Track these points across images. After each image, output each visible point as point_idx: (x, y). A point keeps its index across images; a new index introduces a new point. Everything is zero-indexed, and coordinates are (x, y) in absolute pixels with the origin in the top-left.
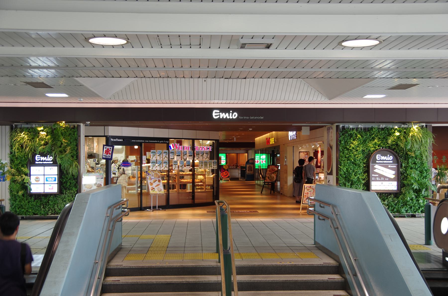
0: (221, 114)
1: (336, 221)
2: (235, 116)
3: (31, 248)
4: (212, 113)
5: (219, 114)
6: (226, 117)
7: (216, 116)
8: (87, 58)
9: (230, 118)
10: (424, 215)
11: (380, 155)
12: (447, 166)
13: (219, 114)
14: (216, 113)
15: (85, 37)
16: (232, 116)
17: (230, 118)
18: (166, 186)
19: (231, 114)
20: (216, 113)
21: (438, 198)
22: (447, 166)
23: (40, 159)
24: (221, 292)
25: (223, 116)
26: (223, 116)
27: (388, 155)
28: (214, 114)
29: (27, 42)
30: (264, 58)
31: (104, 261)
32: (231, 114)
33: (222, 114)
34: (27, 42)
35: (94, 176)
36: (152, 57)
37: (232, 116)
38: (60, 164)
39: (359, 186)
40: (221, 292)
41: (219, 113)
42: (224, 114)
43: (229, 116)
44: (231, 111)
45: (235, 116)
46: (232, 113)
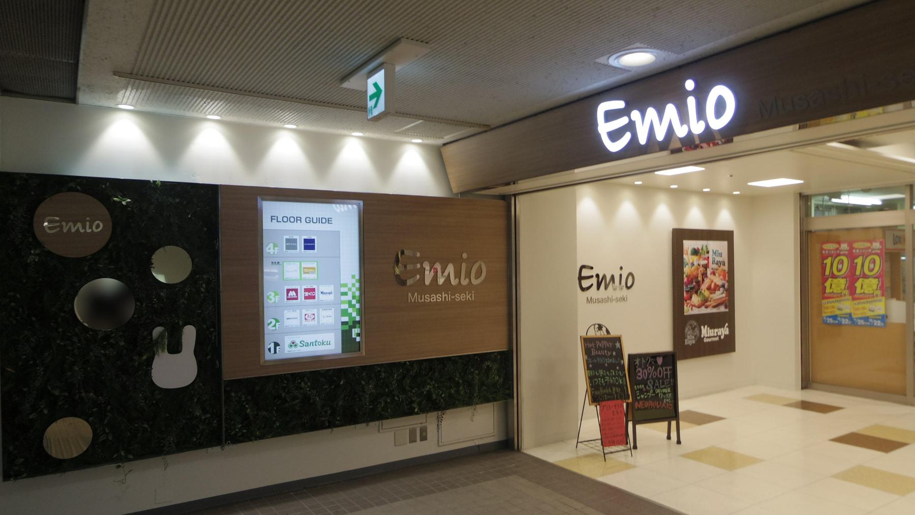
0: (635, 115)
3: (850, 196)
5: (624, 121)
6: (670, 131)
9: (690, 132)
10: (669, 391)
11: (620, 104)
12: (268, 294)
14: (611, 116)
17: (690, 132)
18: (901, 291)
20: (611, 116)
22: (268, 294)
23: (627, 137)
24: (269, 208)
27: (690, 85)
32: (691, 101)
36: (516, 374)
37: (701, 114)
38: (397, 265)
39: (14, 233)
40: (269, 208)
44: (690, 85)
46: (701, 94)
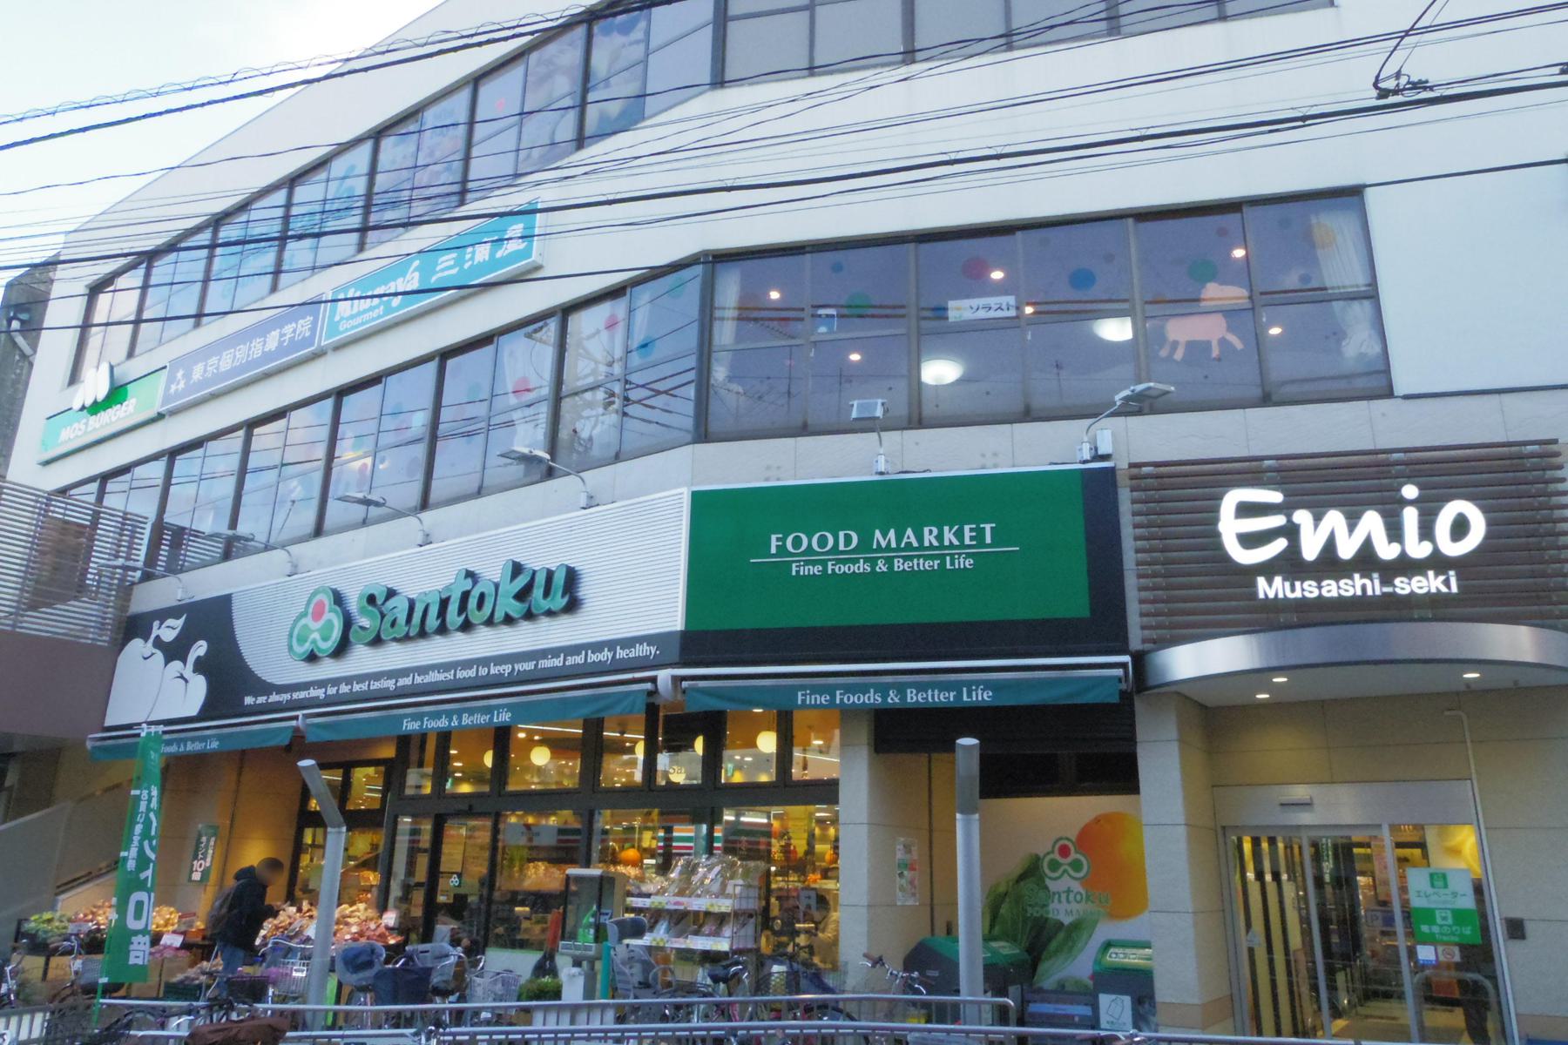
0: (1302, 517)
1: (531, 999)
2: (1460, 528)
4: (1215, 511)
5: (1277, 521)
7: (1249, 541)
8: (563, 116)
9: (1403, 554)
13: (1277, 521)
15: (631, 417)
16: (1426, 532)
17: (1403, 554)
19: (1410, 516)
20: (1245, 510)
21: (221, 543)
23: (1280, 544)
25: (1316, 526)
26: (1316, 526)
28: (1230, 527)
29: (680, 429)
30: (1016, 54)
31: (1236, 574)
32: (1410, 516)
33: (1318, 519)
34: (680, 429)
35: (1082, 581)
37: (1426, 532)
41: (1286, 508)
42: (1335, 519)
43: (1395, 532)
45: (1460, 528)
